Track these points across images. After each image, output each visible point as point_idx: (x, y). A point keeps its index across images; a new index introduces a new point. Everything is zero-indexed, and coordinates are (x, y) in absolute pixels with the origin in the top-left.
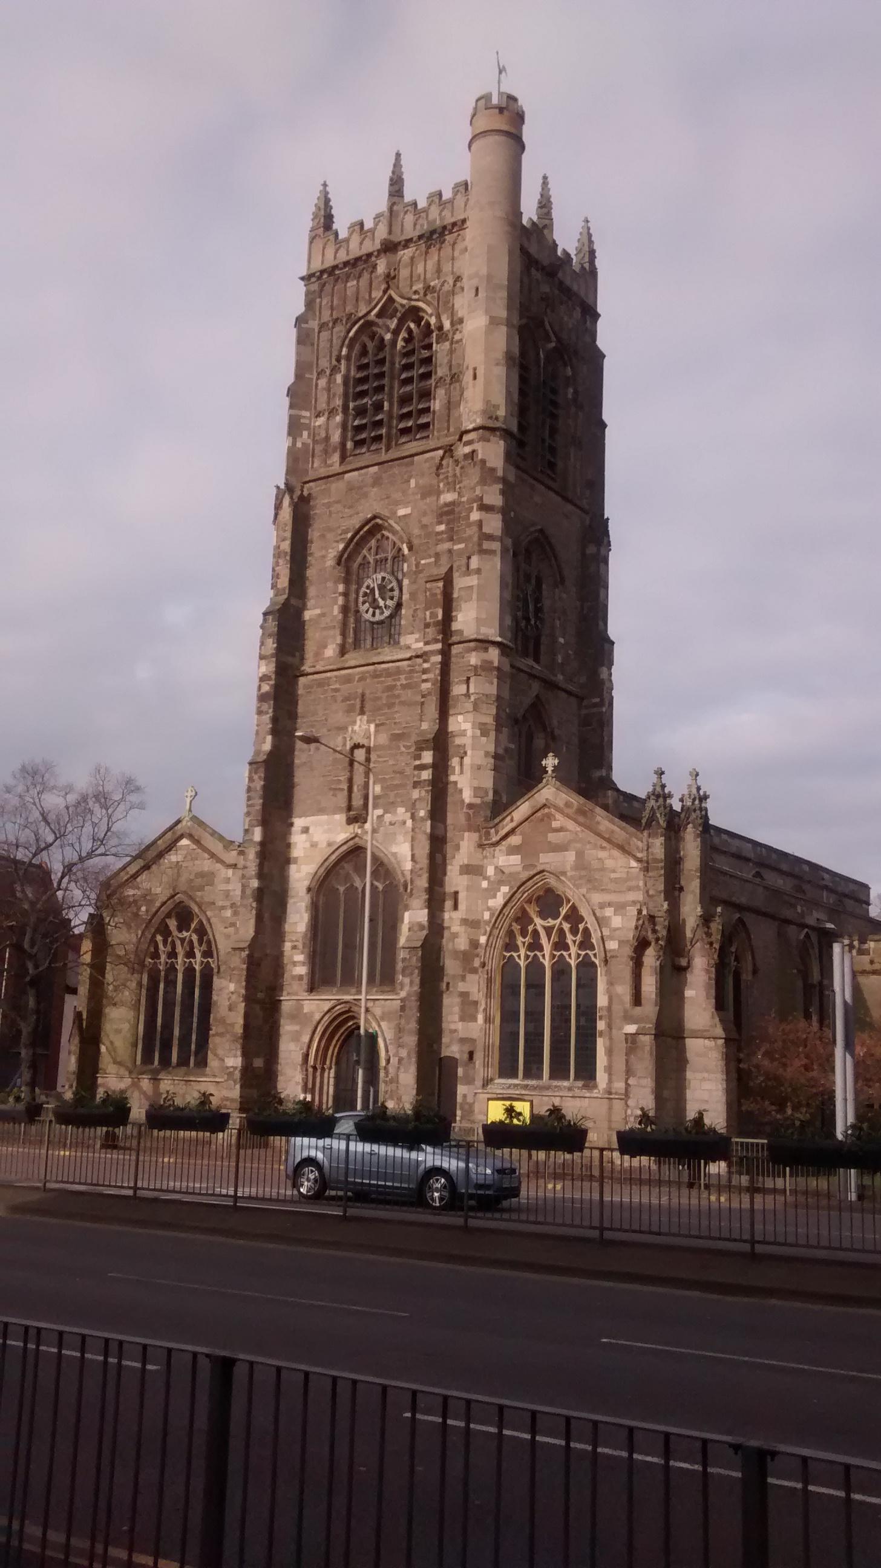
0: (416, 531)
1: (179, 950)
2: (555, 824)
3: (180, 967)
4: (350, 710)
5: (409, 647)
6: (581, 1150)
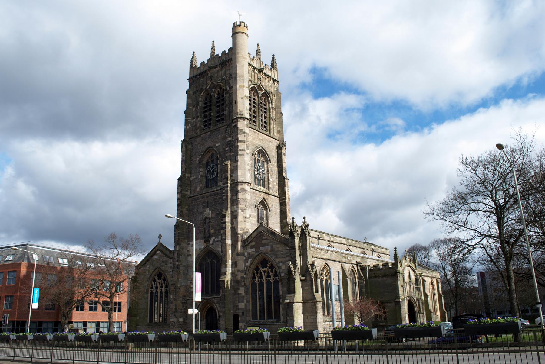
0: (221, 150)
1: (159, 286)
2: (264, 238)
3: (159, 291)
4: (204, 207)
5: (220, 186)
6: (334, 339)
